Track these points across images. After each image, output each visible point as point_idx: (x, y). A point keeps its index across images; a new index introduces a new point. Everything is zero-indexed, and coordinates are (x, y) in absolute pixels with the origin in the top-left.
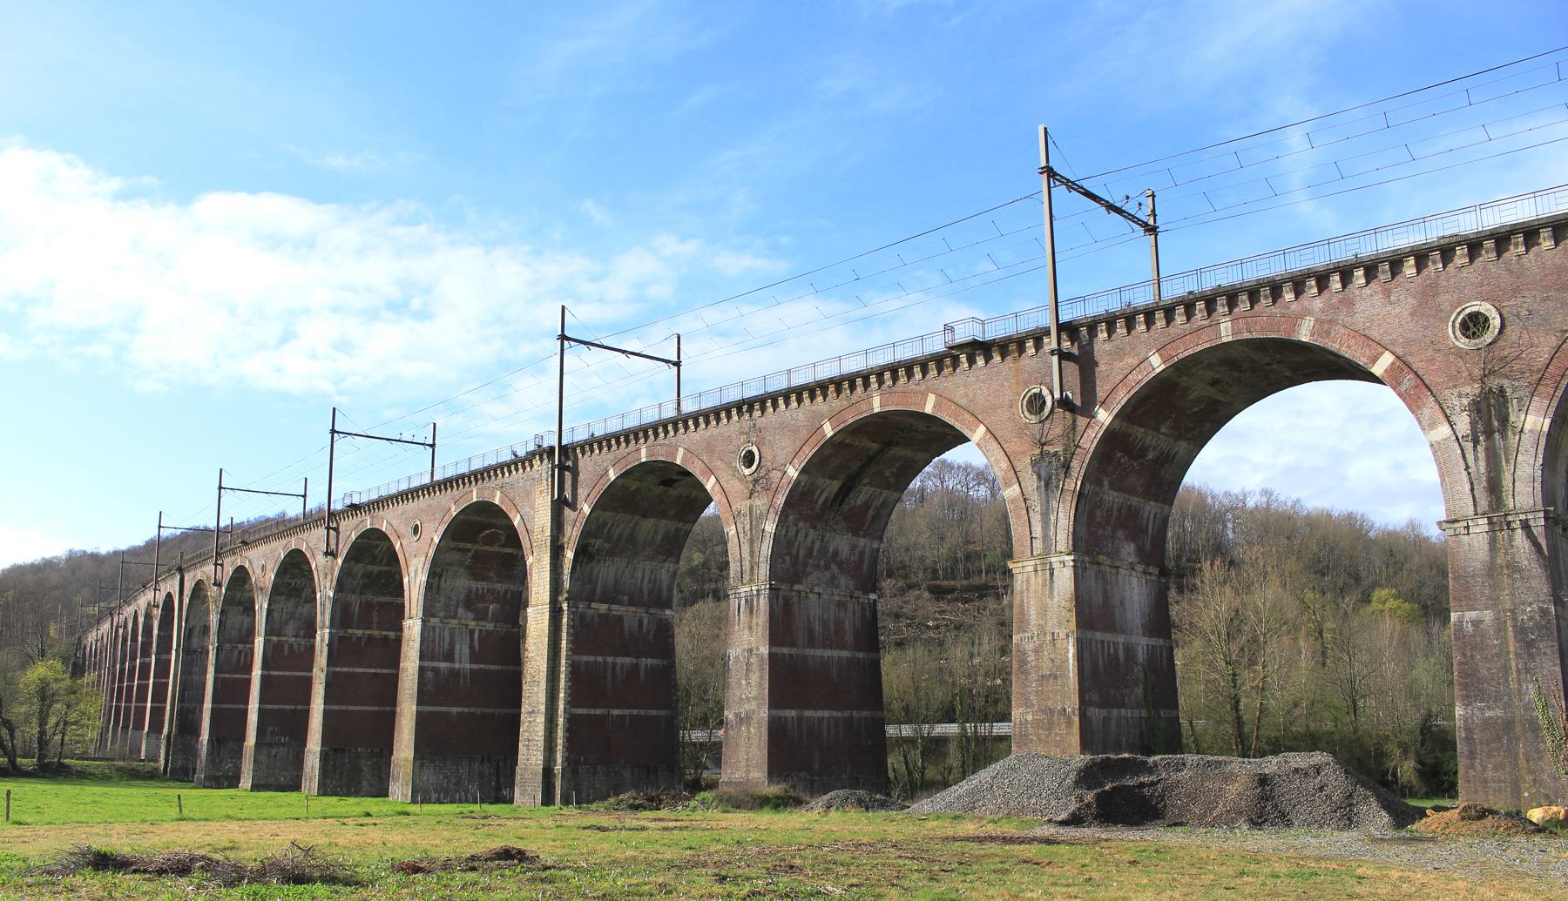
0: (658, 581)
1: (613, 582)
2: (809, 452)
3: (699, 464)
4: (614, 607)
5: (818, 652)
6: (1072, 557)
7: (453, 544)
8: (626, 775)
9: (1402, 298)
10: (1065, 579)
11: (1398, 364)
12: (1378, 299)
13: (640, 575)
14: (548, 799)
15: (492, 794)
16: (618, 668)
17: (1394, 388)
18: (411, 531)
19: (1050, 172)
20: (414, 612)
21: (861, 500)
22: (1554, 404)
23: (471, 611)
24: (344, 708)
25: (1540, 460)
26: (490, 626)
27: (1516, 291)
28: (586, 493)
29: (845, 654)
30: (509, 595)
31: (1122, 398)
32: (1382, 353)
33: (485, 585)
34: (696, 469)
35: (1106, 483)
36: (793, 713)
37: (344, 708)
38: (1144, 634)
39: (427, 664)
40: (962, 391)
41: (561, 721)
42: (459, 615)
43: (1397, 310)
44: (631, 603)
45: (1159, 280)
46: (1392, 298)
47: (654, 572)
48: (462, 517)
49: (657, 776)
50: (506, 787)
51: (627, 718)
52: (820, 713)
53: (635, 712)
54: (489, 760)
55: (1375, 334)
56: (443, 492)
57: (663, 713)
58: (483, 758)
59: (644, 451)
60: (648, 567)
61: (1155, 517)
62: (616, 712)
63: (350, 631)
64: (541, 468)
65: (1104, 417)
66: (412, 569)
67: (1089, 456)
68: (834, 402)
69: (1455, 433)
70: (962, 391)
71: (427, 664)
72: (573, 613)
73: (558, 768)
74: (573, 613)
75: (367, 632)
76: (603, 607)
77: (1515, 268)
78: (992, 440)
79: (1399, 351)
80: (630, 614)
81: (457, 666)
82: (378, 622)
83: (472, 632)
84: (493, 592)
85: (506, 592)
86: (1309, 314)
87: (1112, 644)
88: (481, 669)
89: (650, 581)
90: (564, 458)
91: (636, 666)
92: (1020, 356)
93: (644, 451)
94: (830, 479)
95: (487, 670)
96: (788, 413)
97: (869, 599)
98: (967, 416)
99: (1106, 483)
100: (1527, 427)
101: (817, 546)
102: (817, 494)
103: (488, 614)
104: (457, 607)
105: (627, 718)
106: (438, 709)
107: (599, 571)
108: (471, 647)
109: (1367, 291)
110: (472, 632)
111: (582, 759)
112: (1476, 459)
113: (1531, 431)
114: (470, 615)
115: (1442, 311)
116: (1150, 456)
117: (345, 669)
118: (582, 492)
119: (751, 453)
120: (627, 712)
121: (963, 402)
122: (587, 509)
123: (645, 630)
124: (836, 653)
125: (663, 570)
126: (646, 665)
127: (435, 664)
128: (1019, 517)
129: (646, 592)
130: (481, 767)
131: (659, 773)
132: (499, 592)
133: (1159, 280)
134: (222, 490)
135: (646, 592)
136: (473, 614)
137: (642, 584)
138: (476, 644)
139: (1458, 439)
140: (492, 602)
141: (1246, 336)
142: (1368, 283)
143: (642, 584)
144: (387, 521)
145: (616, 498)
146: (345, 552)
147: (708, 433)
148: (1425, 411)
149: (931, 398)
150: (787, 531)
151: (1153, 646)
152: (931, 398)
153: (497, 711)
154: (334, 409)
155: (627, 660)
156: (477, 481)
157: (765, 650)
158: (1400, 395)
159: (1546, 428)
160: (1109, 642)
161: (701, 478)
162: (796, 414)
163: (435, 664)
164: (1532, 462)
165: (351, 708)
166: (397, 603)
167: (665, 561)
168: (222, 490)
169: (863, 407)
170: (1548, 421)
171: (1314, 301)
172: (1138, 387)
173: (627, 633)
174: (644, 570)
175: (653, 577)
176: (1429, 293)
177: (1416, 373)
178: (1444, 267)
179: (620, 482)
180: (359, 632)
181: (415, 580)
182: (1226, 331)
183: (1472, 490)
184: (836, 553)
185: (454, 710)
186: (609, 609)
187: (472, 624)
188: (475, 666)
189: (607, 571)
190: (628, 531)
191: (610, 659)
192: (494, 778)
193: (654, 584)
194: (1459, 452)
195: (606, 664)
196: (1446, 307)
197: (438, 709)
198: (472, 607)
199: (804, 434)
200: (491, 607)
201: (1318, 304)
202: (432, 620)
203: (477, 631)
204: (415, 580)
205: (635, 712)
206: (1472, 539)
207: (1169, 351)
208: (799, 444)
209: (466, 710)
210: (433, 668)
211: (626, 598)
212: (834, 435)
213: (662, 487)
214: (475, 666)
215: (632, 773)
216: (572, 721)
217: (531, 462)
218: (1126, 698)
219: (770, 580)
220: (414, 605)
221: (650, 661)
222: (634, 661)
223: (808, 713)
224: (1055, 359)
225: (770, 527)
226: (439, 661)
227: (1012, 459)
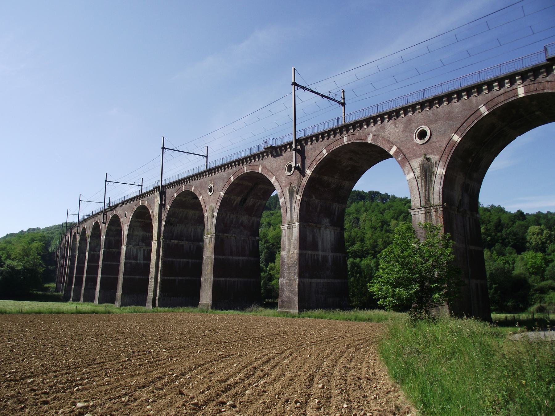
2: (227, 187)
3: (198, 191)
4: (180, 241)
5: (234, 258)
6: (298, 224)
7: (136, 220)
9: (400, 125)
10: (296, 231)
11: (398, 150)
12: (392, 126)
14: (154, 305)
17: (396, 159)
18: (124, 215)
19: (295, 84)
20: (124, 244)
21: (251, 204)
22: (447, 164)
24: (108, 276)
25: (442, 186)
27: (436, 121)
28: (169, 202)
29: (245, 258)
31: (314, 165)
32: (393, 146)
34: (197, 194)
35: (314, 196)
36: (223, 279)
37: (108, 276)
38: (332, 252)
39: (127, 261)
40: (269, 164)
41: (159, 281)
42: (140, 244)
43: (398, 130)
44: (187, 240)
45: (345, 116)
46: (397, 126)
48: (138, 210)
52: (234, 279)
53: (187, 278)
55: (391, 139)
56: (223, 170)
59: (245, 169)
61: (338, 209)
63: (111, 250)
64: (157, 194)
65: (309, 172)
66: (124, 228)
67: (304, 187)
68: (231, 170)
69: (415, 176)
70: (269, 164)
71: (127, 261)
72: (164, 243)
73: (157, 297)
74: (164, 243)
75: (117, 250)
76: (176, 242)
77: (435, 112)
78: (277, 182)
79: (398, 145)
80: (186, 244)
81: (138, 262)
86: (371, 133)
87: (316, 255)
90: (162, 190)
92: (286, 151)
93: (245, 169)
94: (237, 196)
96: (222, 173)
97: (256, 239)
98: (270, 173)
99: (314, 196)
100: (438, 173)
101: (234, 220)
102: (232, 202)
104: (139, 241)
106: (131, 277)
108: (144, 255)
109: (389, 123)
111: (166, 294)
112: (422, 186)
113: (439, 174)
114: (144, 244)
115: (412, 130)
116: (333, 186)
117: (109, 263)
118: (167, 201)
119: (211, 187)
120: (184, 278)
121: (269, 168)
122: (168, 208)
124: (242, 258)
127: (131, 261)
128: (284, 209)
129: (192, 236)
133: (345, 116)
134: (107, 182)
135: (192, 236)
137: (191, 233)
138: (146, 255)
139: (416, 178)
141: (352, 141)
142: (389, 121)
144: (119, 212)
145: (176, 203)
146: (108, 222)
147: (200, 181)
148: (406, 168)
149: (260, 167)
150: (222, 215)
151: (336, 256)
152: (260, 167)
154: (107, 173)
155: (185, 260)
156: (247, 162)
157: (213, 257)
158: (398, 162)
159: (444, 173)
160: (314, 255)
161: (198, 196)
162: (223, 174)
163: (131, 261)
164: (439, 186)
165: (111, 276)
168: (107, 182)
169: (255, 167)
170: (444, 171)
171: (373, 128)
172: (319, 161)
176: (408, 123)
177: (403, 153)
178: (413, 113)
179: (178, 197)
180: (114, 250)
181: (125, 232)
182: (346, 140)
183: (420, 197)
184: (242, 222)
185: (137, 277)
186: (178, 242)
188: (145, 262)
189: (178, 229)
194: (416, 183)
196: (413, 128)
197: (131, 277)
199: (226, 180)
201: (374, 129)
202: (130, 246)
203: (146, 250)
204: (125, 232)
205: (187, 278)
206: (419, 216)
207: (329, 148)
208: (224, 184)
209: (141, 277)
210: (130, 262)
211: (185, 238)
212: (234, 181)
213: (194, 200)
214: (145, 262)
216: (162, 281)
217: (155, 191)
218: (322, 275)
219: (215, 232)
220: (124, 241)
222: (187, 260)
223: (228, 279)
224: (294, 152)
225: (216, 213)
226: (132, 260)
227: (282, 188)
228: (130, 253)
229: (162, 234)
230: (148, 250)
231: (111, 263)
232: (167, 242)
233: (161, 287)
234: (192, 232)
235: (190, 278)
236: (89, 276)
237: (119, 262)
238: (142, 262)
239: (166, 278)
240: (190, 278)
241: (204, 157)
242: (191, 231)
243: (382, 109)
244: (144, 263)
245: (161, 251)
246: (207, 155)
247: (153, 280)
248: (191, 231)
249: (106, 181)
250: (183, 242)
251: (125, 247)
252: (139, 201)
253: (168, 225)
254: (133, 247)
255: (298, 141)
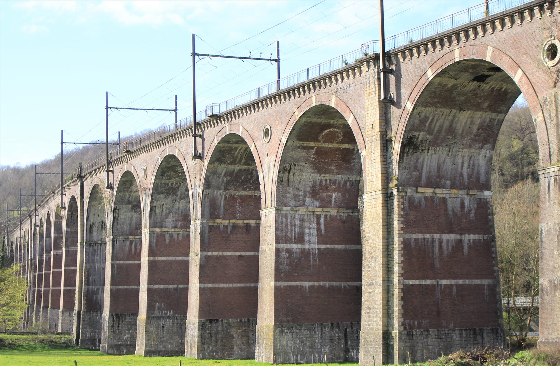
0: (476, 167)
1: (436, 170)
4: (438, 190)
7: (298, 143)
8: (455, 337)
13: (460, 161)
15: (342, 355)
16: (444, 244)
23: (317, 200)
26: (334, 212)
28: (409, 92)
30: (348, 184)
33: (327, 177)
39: (281, 246)
44: (453, 187)
47: (473, 157)
48: (304, 119)
49: (483, 337)
50: (353, 349)
51: (454, 287)
53: (461, 281)
54: (338, 327)
57: (485, 282)
58: (332, 324)
60: (467, 154)
62: (444, 282)
63: (218, 221)
73: (395, 332)
74: (402, 197)
75: (232, 221)
81: (307, 246)
82: (241, 213)
83: (318, 218)
84: (334, 182)
85: (346, 182)
88: (327, 249)
89: (469, 166)
91: (460, 241)
95: (333, 250)
103: (331, 201)
105: (454, 287)
106: (293, 284)
107: (424, 159)
108: (319, 230)
110: (318, 218)
114: (316, 203)
117: (215, 253)
120: (454, 282)
123: (466, 210)
125: (481, 156)
126: (469, 240)
127: (289, 246)
129: (465, 176)
130: (331, 332)
131: (485, 335)
132: (340, 183)
134: (196, 57)
135: (465, 176)
136: (318, 203)
137: (462, 168)
138: (322, 227)
140: (334, 191)
143: (462, 168)
149: (490, 50)
152: (490, 50)
153: (343, 284)
163: (289, 246)
165: (222, 285)
166: (255, 196)
167: (482, 148)
173: (450, 213)
174: (463, 157)
175: (472, 163)
179: (438, 80)
180: (226, 222)
185: (306, 284)
186: (434, 193)
187: (318, 211)
188: (322, 247)
190: (447, 123)
191: (437, 236)
192: (343, 341)
193: (473, 169)
195: (433, 241)
197: (293, 284)
198: (318, 196)
200: (334, 195)
205: (461, 281)
209: (316, 284)
211: (448, 182)
214: (322, 247)
215: (461, 334)
221: (472, 237)
222: (458, 237)
226: (292, 243)
228: (287, 226)
229: (396, 173)
230: (328, 218)
231: (221, 253)
232: (409, 194)
233: (403, 306)
234: (466, 165)
235: (467, 282)
236: (252, 285)
237: (361, 244)
238: (316, 246)
239: (412, 282)
240: (467, 282)
241: (273, 62)
242: (463, 163)
243: (398, 44)
244: (319, 249)
245: (396, 217)
246: (279, 58)
247: (379, 290)
248: (463, 163)
249: (194, 54)
250: (445, 191)
251: (273, 211)
252: (310, 96)
253: (407, 150)
254: (293, 210)
255: (387, 56)
